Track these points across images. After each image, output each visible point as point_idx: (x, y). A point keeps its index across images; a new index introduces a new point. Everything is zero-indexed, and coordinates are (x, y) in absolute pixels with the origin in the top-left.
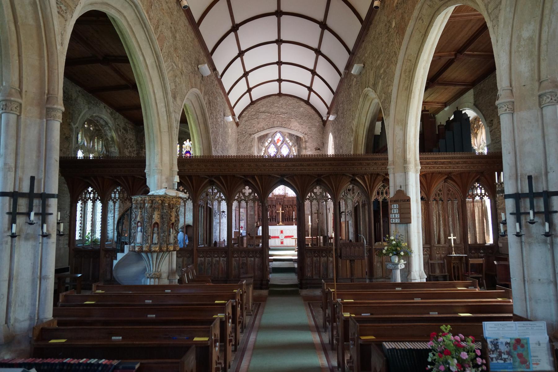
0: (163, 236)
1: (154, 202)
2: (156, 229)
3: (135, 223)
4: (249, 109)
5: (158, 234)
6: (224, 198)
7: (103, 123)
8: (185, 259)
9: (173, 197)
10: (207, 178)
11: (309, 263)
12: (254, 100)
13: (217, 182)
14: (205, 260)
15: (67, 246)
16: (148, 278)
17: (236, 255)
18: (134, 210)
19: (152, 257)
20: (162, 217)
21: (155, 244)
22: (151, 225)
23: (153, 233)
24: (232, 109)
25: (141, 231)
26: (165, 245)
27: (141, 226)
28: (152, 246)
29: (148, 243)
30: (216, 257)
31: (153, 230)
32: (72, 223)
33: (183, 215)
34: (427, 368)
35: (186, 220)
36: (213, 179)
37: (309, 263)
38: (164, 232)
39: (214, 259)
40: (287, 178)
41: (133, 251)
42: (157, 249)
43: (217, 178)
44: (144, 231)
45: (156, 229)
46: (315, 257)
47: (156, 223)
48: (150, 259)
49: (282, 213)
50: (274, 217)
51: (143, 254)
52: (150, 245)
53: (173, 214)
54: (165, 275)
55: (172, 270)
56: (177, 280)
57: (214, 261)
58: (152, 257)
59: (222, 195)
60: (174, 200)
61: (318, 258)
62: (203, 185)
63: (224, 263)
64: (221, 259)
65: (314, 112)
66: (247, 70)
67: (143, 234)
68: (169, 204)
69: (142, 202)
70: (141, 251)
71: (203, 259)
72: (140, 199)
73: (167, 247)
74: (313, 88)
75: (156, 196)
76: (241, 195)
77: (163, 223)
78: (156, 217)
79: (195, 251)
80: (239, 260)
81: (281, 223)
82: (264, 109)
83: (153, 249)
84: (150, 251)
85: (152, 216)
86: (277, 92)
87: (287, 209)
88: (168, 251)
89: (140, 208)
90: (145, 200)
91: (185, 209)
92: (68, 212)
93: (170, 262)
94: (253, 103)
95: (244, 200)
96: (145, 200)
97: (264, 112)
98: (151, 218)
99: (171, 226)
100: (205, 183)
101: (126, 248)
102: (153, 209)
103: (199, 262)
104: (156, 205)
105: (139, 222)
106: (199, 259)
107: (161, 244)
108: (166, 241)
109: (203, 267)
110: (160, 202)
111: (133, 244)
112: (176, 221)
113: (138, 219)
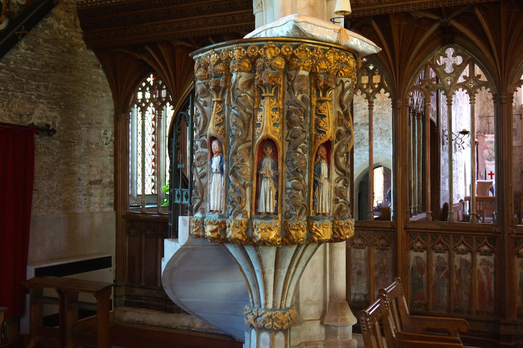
0: (294, 188)
1: (259, 63)
2: (268, 162)
3: (204, 145)
5: (276, 179)
6: (484, 78)
8: (375, 251)
9: (328, 46)
10: (433, 21)
15: (111, 209)
16: (252, 326)
17: (418, 244)
18: (201, 100)
19: (260, 259)
20: (288, 121)
21: (268, 216)
22: (250, 149)
23: (259, 178)
25: (221, 171)
26: (303, 223)
27: (220, 152)
28: (256, 222)
29: (240, 211)
30: (464, 252)
31: (260, 167)
32: (120, 156)
33: (367, 144)
34: (152, 76)
35: (375, 156)
36: (453, 23)
38: (296, 173)
39: (457, 258)
41: (197, 236)
42: (273, 235)
44: (230, 172)
45: (268, 162)
47: (268, 141)
48: (256, 268)
51: (232, 250)
52: (251, 219)
53: (331, 111)
54: (311, 311)
55: (333, 295)
56: (350, 329)
57: (457, 263)
58: (260, 259)
59: (478, 71)
60: (331, 57)
62: (419, 45)
63: (486, 271)
64: (479, 258)
67: (227, 178)
68: (313, 74)
69: (220, 67)
70: (221, 240)
71: (423, 255)
72: (214, 57)
73: (309, 227)
75: (267, 40)
77: (293, 140)
78: (267, 121)
79: (401, 232)
83: (258, 235)
84: (248, 241)
85: (252, 117)
88: (312, 239)
89: (217, 89)
90: (229, 59)
91: (371, 129)
92: (110, 134)
93: (328, 271)
96: (229, 59)
98: (250, 122)
99: (323, 151)
100: (426, 36)
101: (184, 224)
102: (258, 89)
103: (412, 263)
104: (265, 77)
105: (213, 138)
106: (413, 254)
107: (287, 216)
108: (307, 207)
109: (424, 276)
110: (280, 62)
111: (198, 215)
112: (339, 134)
113: (211, 129)
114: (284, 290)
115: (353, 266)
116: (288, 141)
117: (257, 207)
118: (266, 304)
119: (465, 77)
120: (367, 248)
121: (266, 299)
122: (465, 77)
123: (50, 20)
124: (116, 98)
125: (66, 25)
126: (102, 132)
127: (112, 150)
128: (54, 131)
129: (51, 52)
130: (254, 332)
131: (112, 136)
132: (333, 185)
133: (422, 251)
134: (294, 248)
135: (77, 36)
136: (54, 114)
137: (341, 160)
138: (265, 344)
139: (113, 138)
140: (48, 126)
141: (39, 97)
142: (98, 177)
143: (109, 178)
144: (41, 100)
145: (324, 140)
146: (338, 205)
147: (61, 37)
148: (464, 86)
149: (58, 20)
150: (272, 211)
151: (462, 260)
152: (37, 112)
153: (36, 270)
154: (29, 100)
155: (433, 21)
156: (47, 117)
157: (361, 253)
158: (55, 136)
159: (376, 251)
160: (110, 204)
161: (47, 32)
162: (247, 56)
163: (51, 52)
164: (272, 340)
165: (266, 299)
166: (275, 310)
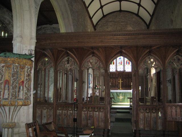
2: (7, 86)
4: (102, 20)
7: (8, 22)
11: (142, 118)
12: (105, 14)
13: (71, 54)
14: (62, 113)
17: (60, 109)
24: (91, 18)
37: (142, 118)
40: (125, 50)
43: (71, 49)
45: (7, 86)
46: (147, 113)
49: (122, 82)
50: (117, 85)
57: (69, 113)
61: (149, 114)
65: (141, 20)
66: (102, 5)
71: (61, 111)
74: (142, 4)
76: (89, 64)
80: (87, 113)
81: (121, 89)
82: (111, 20)
86: (119, 9)
87: (125, 80)
94: (104, 16)
95: (92, 68)
97: (111, 22)
103: (58, 113)
106: (58, 111)
109: (61, 117)
114: (12, 117)
117: (3, 96)
119: (154, 64)
120: (47, 110)
121: (7, 120)
122: (154, 64)
130: (4, 129)
132: (25, 92)
134: (14, 107)
137: (27, 86)
145: (21, 81)
148: (154, 67)
150: (7, 98)
151: (59, 112)
155: (64, 51)
159: (49, 110)
162: (3, 60)
164: (8, 131)
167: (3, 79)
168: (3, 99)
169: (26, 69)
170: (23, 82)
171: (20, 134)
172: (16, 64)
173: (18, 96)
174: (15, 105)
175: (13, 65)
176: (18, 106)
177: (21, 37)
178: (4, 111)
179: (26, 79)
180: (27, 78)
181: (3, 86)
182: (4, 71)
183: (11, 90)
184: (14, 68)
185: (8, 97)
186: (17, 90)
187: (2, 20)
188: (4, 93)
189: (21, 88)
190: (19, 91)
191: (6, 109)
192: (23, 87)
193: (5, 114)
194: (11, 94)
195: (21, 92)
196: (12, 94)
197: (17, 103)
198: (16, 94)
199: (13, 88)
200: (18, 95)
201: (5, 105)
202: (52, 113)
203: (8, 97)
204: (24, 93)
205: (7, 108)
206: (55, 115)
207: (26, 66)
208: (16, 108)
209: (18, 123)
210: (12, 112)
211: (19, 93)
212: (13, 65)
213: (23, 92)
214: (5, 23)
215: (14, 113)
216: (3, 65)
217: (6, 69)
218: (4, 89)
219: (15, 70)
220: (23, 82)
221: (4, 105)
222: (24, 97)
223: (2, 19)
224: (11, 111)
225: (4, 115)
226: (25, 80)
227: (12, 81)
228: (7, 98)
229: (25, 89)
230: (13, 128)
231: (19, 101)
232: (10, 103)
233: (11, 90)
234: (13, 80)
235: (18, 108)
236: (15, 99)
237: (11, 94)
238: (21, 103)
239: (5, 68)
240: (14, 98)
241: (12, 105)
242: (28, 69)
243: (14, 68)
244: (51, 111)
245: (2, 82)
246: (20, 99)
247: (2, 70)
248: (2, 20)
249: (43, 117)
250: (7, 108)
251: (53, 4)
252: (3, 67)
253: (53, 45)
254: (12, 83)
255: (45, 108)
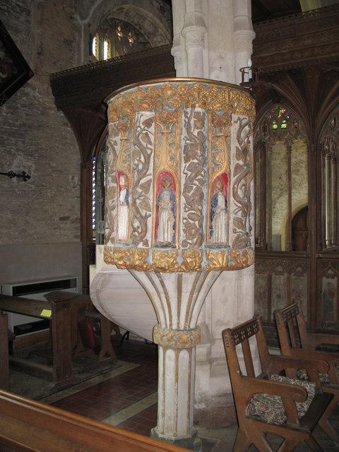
2: (166, 195)
7: (150, 29)
15: (79, 240)
17: (330, 272)
45: (166, 195)
92: (77, 179)
103: (324, 287)
106: (325, 280)
114: (187, 313)
115: (274, 290)
116: (185, 174)
117: (156, 237)
118: (171, 325)
121: (171, 320)
123: (26, 89)
124: (82, 149)
125: (40, 93)
126: (71, 177)
127: (79, 192)
128: (29, 177)
129: (27, 114)
131: (78, 181)
133: (333, 278)
134: (194, 275)
135: (49, 100)
136: (29, 164)
137: (240, 193)
138: (170, 359)
139: (80, 183)
140: (24, 173)
141: (18, 150)
142: (67, 214)
143: (77, 214)
144: (19, 153)
145: (219, 173)
146: (236, 235)
147: (35, 102)
149: (34, 89)
150: (170, 240)
152: (16, 162)
153: (13, 288)
154: (9, 152)
156: (24, 167)
157: (280, 280)
158: (29, 181)
159: (294, 277)
160: (76, 237)
161: (24, 99)
163: (27, 114)
164: (177, 357)
165: (171, 320)
166: (178, 331)
167: (151, 171)
168: (156, 246)
169: (234, 129)
170: (225, 178)
171: (215, 363)
172: (198, 109)
173: (212, 232)
174: (200, 267)
175: (186, 113)
176: (209, 272)
177: (201, 22)
178: (161, 289)
179: (237, 167)
180: (241, 162)
181: (151, 196)
182: (152, 138)
183: (182, 211)
184: (188, 125)
185: (174, 236)
186: (206, 210)
187: (136, 25)
188: (157, 225)
189: (221, 200)
190: (212, 214)
191: (166, 283)
192: (226, 197)
193: (163, 296)
194: (181, 223)
195: (221, 220)
196: (188, 228)
197: (208, 259)
198: (201, 226)
199: (190, 204)
200: (211, 227)
201: (164, 270)
202: (302, 284)
203: (174, 236)
204: (231, 221)
205: (170, 280)
206: (315, 295)
207: (235, 117)
208: (201, 278)
209: (207, 327)
210: (188, 294)
211: (212, 220)
212: (186, 113)
213: (228, 218)
214: (142, 32)
215: (194, 296)
216: (148, 115)
217: (159, 132)
218: (158, 207)
219: (195, 133)
220: (225, 178)
221: (162, 268)
222: (233, 236)
223: (136, 21)
224: (184, 289)
225: (162, 304)
226: (232, 169)
227: (183, 176)
228: (170, 240)
229: (233, 205)
230: (193, 349)
231: (215, 251)
232: (180, 260)
233: (182, 211)
234: (189, 173)
235: (208, 279)
236: (201, 245)
237: (181, 223)
238: (220, 261)
239: (156, 125)
240: (195, 240)
241: (189, 268)
242: (242, 127)
243: (188, 125)
244: (302, 280)
245: (150, 181)
246: (219, 246)
247: (146, 134)
248: (136, 25)
249: (274, 297)
250: (170, 280)
251: (105, 312)
252: (148, 123)
253: (306, 54)
254: (183, 182)
255: (280, 269)
